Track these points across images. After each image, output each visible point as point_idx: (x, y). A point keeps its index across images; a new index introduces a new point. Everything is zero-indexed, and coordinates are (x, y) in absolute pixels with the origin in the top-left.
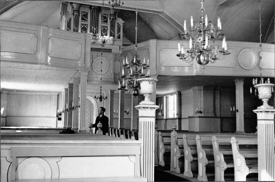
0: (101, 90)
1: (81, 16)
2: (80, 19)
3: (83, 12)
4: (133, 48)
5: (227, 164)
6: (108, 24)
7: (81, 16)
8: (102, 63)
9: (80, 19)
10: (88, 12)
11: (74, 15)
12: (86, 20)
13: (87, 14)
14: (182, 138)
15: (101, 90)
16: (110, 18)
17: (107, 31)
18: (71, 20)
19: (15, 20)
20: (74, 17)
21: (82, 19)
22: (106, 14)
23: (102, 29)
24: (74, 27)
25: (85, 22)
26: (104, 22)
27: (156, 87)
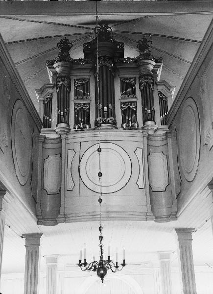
0: (101, 238)
1: (73, 88)
2: (72, 94)
3: (78, 80)
4: (157, 124)
5: (38, 223)
6: (136, 98)
7: (73, 88)
8: (100, 174)
9: (72, 94)
10: (89, 79)
11: (57, 88)
12: (85, 95)
13: (88, 83)
14: (117, 254)
15: (101, 238)
16: (140, 84)
17: (136, 111)
18: (51, 99)
19: (81, 181)
20: (58, 90)
21: (77, 94)
22: (132, 78)
23: (123, 110)
24: (58, 111)
25: (82, 99)
26: (127, 94)
27: (49, 128)
